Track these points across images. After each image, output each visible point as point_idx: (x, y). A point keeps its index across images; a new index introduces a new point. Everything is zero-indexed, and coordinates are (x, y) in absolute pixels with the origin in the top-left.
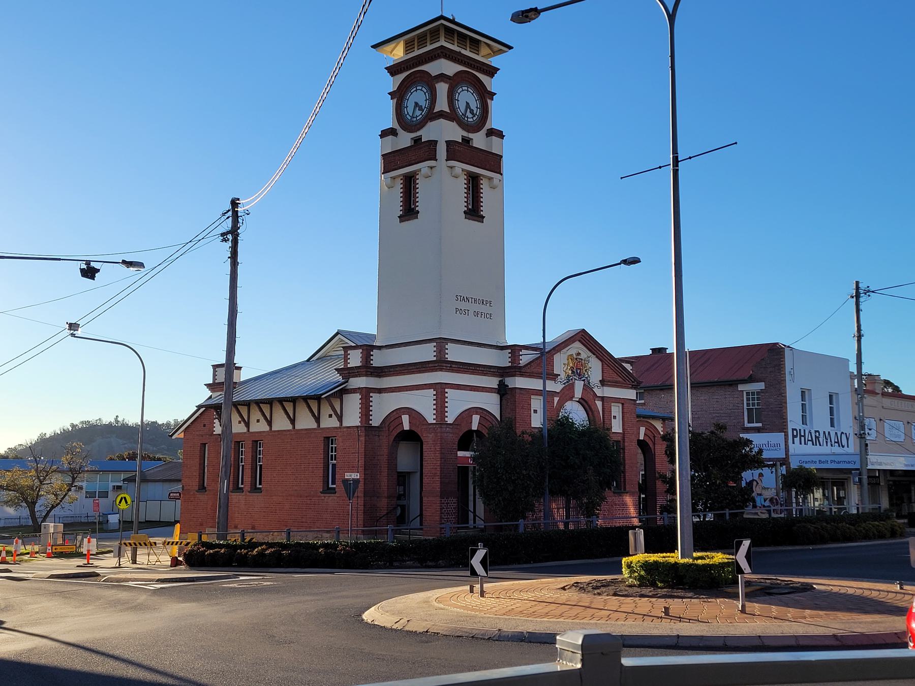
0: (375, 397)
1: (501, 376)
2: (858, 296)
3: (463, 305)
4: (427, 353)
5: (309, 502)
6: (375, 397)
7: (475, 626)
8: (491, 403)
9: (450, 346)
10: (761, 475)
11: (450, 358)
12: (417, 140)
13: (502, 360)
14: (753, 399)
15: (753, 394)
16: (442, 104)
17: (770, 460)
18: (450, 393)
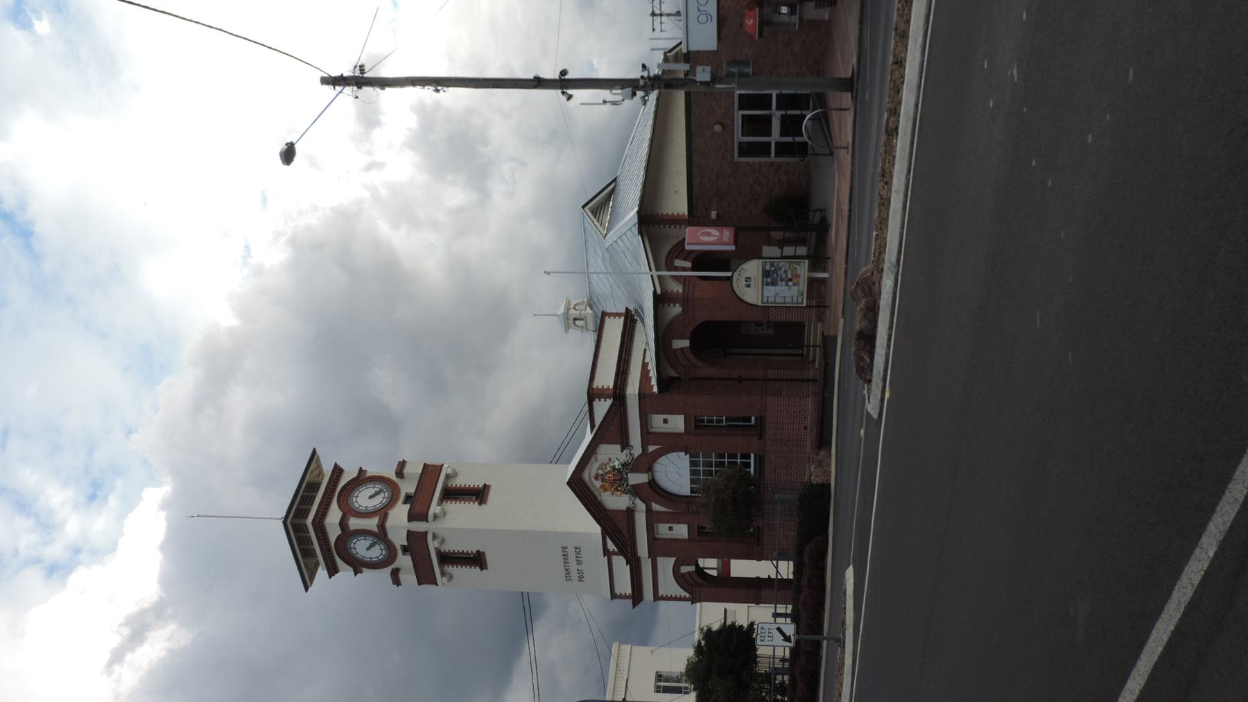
3: (575, 575)
12: (405, 549)
13: (620, 563)
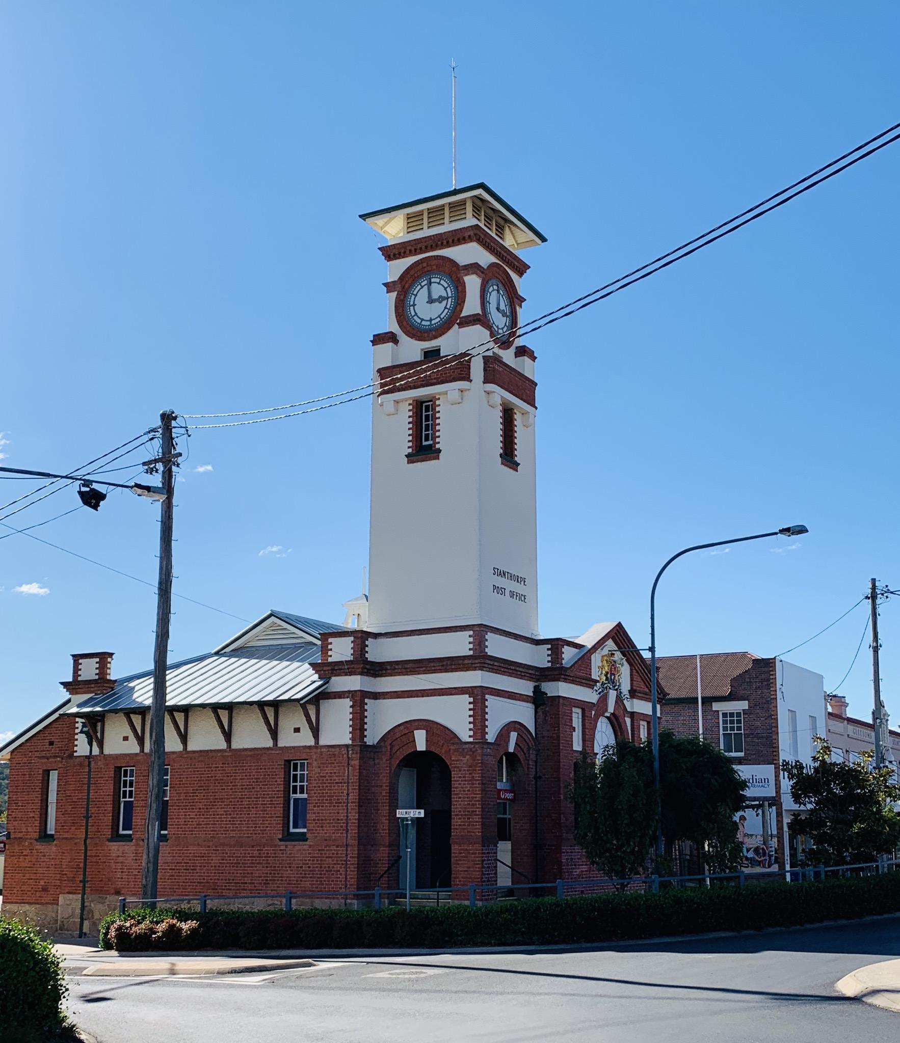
0: (370, 703)
1: (537, 680)
2: (873, 597)
3: (501, 582)
4: (460, 645)
5: (256, 853)
6: (370, 703)
7: (841, 1007)
8: (525, 714)
9: (490, 636)
10: (743, 818)
11: (490, 651)
13: (540, 658)
14: (732, 722)
15: (732, 715)
16: (472, 307)
17: (755, 799)
18: (491, 701)
